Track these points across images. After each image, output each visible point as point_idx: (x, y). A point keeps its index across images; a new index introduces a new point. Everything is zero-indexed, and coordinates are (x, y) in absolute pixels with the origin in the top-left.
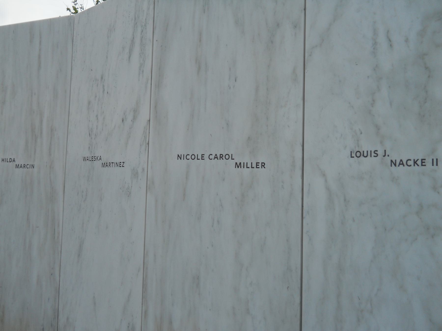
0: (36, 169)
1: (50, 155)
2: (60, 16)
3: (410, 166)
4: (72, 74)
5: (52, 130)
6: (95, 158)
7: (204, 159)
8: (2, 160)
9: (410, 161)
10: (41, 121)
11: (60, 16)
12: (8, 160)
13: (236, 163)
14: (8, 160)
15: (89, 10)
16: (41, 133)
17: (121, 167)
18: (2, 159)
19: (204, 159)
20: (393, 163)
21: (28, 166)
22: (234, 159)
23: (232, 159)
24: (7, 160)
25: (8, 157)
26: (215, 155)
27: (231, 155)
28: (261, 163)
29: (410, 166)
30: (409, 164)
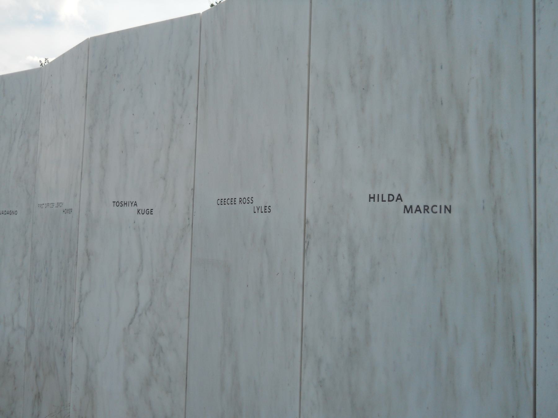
0: (455, 216)
1: (491, 185)
2: (212, 5)
3: (436, 212)
4: (539, 21)
5: (491, 137)
6: (270, 209)
7: (152, 214)
8: (370, 198)
9: (435, 207)
10: (463, 121)
11: (212, 5)
12: (386, 198)
13: (405, 207)
14: (386, 198)
15: (51, 62)
16: (465, 142)
17: (232, 204)
18: (370, 195)
19: (152, 214)
20: (407, 209)
21: (435, 209)
22: (113, 202)
23: (383, 201)
24: (382, 199)
25: (384, 190)
26: (416, 207)
27: (405, 212)
28: (383, 202)
29: (436, 212)
30: (434, 211)
